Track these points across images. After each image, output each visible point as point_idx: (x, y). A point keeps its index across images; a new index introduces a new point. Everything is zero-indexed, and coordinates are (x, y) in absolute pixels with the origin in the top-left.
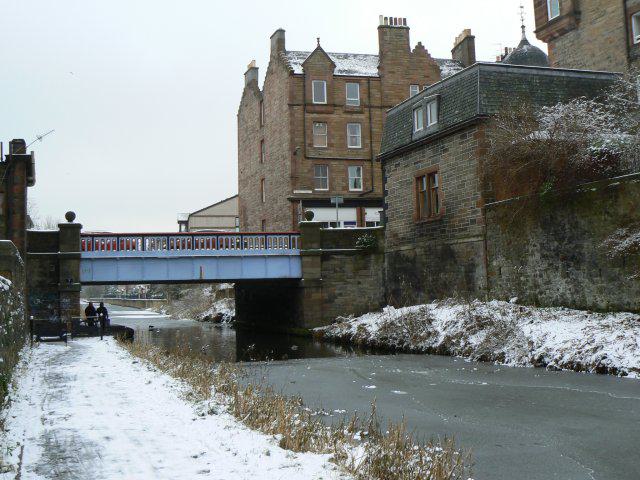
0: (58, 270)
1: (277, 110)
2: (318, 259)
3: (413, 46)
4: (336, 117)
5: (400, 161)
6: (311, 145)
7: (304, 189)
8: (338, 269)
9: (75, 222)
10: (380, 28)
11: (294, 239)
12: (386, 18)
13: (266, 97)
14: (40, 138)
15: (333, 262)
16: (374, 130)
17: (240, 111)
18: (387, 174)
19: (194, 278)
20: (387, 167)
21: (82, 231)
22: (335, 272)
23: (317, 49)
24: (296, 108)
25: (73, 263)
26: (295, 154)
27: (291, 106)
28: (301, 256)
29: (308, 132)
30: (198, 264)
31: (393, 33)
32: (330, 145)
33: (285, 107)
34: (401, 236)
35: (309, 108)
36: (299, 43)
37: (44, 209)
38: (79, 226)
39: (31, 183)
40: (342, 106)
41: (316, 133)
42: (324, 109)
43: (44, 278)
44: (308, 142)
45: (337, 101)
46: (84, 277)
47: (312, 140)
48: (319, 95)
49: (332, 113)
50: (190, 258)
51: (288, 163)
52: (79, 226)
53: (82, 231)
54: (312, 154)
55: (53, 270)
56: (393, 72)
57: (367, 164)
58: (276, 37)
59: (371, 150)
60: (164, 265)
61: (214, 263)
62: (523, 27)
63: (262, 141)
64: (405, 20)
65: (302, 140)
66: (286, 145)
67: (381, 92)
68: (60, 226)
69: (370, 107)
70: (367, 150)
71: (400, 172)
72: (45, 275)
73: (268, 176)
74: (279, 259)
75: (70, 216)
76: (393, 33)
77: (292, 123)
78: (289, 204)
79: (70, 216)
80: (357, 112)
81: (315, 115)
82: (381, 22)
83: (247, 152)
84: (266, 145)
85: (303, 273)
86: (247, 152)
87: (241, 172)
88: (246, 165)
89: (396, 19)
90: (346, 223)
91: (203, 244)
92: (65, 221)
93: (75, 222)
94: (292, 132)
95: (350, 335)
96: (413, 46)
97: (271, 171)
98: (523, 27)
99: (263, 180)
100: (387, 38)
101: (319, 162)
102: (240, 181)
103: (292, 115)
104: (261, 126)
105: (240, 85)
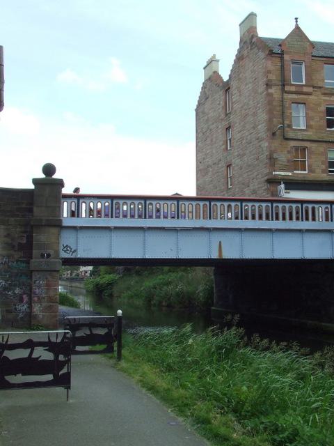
0: (30, 238)
6: (290, 126)
13: (234, 84)
29: (287, 113)
30: (216, 238)
32: (308, 126)
33: (262, 88)
36: (273, 28)
38: (60, 183)
40: (320, 88)
44: (287, 122)
47: (291, 122)
49: (309, 94)
52: (60, 183)
61: (236, 237)
66: (262, 127)
73: (236, 162)
74: (263, 234)
75: (49, 170)
77: (270, 103)
78: (266, 186)
79: (49, 170)
81: (294, 96)
83: (209, 141)
86: (209, 141)
87: (199, 162)
88: (206, 154)
91: (291, 214)
94: (270, 112)
97: (241, 156)
99: (229, 166)
100: (199, 144)
104: (227, 115)
105: (199, 79)
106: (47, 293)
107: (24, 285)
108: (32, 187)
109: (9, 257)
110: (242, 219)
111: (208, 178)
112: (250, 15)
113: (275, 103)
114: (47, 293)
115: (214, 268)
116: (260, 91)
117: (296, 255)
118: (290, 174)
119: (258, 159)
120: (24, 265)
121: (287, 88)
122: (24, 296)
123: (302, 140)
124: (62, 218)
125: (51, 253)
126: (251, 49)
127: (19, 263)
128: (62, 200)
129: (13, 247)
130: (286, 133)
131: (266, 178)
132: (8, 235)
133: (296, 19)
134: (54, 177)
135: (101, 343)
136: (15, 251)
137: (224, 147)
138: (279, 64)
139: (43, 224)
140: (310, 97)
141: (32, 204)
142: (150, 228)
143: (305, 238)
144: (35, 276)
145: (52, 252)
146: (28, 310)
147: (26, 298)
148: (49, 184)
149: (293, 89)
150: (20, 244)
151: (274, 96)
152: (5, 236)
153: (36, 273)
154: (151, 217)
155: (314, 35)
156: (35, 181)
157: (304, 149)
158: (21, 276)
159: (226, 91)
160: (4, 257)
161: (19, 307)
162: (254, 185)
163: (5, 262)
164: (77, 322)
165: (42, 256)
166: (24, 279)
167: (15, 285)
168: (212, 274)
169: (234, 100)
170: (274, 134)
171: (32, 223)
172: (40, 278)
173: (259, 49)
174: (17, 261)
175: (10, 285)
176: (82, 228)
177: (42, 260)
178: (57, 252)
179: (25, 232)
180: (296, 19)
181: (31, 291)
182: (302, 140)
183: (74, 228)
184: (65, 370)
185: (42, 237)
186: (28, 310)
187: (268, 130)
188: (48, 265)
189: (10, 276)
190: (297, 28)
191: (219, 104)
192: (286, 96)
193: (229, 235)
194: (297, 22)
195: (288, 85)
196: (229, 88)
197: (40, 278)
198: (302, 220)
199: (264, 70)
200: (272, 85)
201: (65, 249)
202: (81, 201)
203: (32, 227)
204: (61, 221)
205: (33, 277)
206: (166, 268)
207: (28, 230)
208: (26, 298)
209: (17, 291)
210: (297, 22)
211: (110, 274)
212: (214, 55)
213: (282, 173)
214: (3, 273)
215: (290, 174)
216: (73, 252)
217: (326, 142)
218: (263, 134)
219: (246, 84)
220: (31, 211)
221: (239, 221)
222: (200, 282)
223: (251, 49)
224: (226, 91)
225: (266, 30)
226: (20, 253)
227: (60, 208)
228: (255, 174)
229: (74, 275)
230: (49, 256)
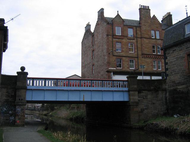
1: (101, 39)
3: (152, 16)
4: (124, 41)
5: (175, 48)
7: (113, 67)
8: (144, 97)
10: (140, 9)
11: (93, 82)
12: (142, 6)
13: (96, 34)
16: (138, 46)
17: (82, 41)
18: (167, 55)
20: (167, 52)
21: (28, 76)
22: (144, 98)
23: (117, 15)
24: (109, 36)
25: (23, 91)
26: (109, 54)
27: (107, 35)
28: (129, 91)
29: (114, 46)
30: (82, 94)
31: (144, 11)
32: (122, 51)
33: (105, 36)
34: (177, 82)
35: (114, 37)
36: (109, 14)
38: (27, 74)
39: (4, 51)
41: (117, 46)
42: (120, 37)
43: (8, 98)
44: (114, 49)
45: (125, 35)
46: (28, 98)
48: (118, 32)
50: (79, 90)
51: (106, 57)
52: (27, 74)
53: (28, 76)
54: (116, 54)
56: (145, 25)
57: (136, 59)
58: (101, 12)
59: (138, 54)
60: (66, 93)
61: (89, 93)
62: (187, 13)
63: (93, 51)
64: (148, 7)
65: (112, 48)
66: (105, 51)
67: (141, 32)
69: (137, 37)
70: (136, 53)
71: (176, 53)
73: (96, 64)
75: (23, 68)
76: (144, 11)
77: (108, 42)
78: (107, 73)
79: (23, 68)
80: (132, 39)
81: (117, 40)
82: (140, 7)
84: (95, 52)
85: (130, 99)
87: (82, 63)
89: (145, 6)
91: (120, 86)
94: (108, 45)
95: (177, 129)
96: (152, 16)
97: (97, 61)
98: (187, 13)
99: (93, 65)
100: (143, 13)
101: (118, 57)
102: (82, 67)
103: (108, 39)
104: (93, 45)
105: (83, 32)
108: (17, 75)
110: (124, 87)
111: (86, 70)
112: (101, 9)
116: (105, 37)
117: (100, 100)
118: (115, 69)
119: (103, 63)
128: (27, 80)
130: (114, 53)
131: (106, 70)
132: (7, 92)
133: (118, 11)
134: (25, 71)
135: (40, 103)
137: (91, 58)
140: (123, 40)
142: (59, 90)
143: (114, 94)
144: (17, 107)
148: (23, 74)
154: (82, 86)
155: (123, 17)
156: (18, 73)
162: (102, 73)
167: (10, 110)
168: (85, 107)
169: (95, 40)
180: (118, 11)
183: (31, 90)
185: (18, 93)
190: (118, 15)
191: (90, 41)
192: (114, 40)
193: (87, 93)
194: (118, 12)
198: (124, 87)
202: (34, 80)
210: (118, 12)
212: (89, 22)
213: (112, 69)
215: (115, 69)
217: (129, 57)
218: (105, 54)
219: (100, 34)
220: (16, 83)
221: (79, 87)
224: (93, 36)
225: (106, 15)
230: (22, 99)
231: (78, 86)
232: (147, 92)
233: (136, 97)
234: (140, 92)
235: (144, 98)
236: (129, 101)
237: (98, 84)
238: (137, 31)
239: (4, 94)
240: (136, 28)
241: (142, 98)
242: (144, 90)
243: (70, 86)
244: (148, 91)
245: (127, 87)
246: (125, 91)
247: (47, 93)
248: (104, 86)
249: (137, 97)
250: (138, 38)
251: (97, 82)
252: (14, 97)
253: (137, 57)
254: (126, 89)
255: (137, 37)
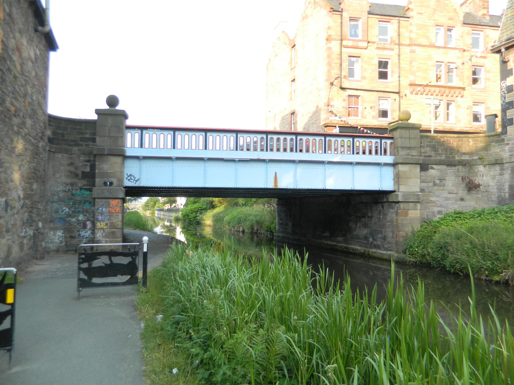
0: (93, 167)
2: (418, 168)
8: (438, 182)
9: (119, 108)
14: (464, 51)
15: (432, 172)
19: (268, 187)
21: (129, 122)
22: (435, 184)
28: (394, 165)
30: (273, 168)
37: (71, 93)
43: (75, 180)
52: (124, 115)
53: (129, 122)
55: (88, 169)
68: (98, 112)
72: (77, 175)
75: (112, 101)
77: (329, 56)
79: (112, 101)
90: (436, 132)
92: (105, 106)
93: (119, 108)
94: (329, 64)
106: (109, 220)
107: (87, 212)
108: (95, 117)
109: (72, 184)
110: (381, 154)
113: (333, 57)
114: (109, 220)
115: (277, 200)
120: (88, 193)
121: (345, 43)
122: (88, 223)
123: (357, 90)
124: (125, 149)
125: (113, 181)
126: (315, 8)
127: (83, 191)
129: (77, 175)
134: (118, 108)
136: (79, 179)
138: (339, 21)
139: (106, 153)
141: (95, 134)
145: (114, 181)
146: (91, 236)
147: (89, 224)
148: (112, 116)
149: (350, 43)
150: (83, 173)
151: (333, 50)
152: (69, 165)
153: (99, 200)
156: (98, 112)
157: (358, 97)
158: (84, 203)
159: (293, 47)
160: (67, 184)
161: (83, 233)
163: (69, 190)
164: (95, 251)
165: (105, 184)
166: (87, 206)
167: (79, 212)
170: (332, 84)
171: (94, 153)
172: (103, 205)
173: (321, 8)
174: (81, 189)
175: (74, 212)
176: (145, 158)
177: (104, 187)
178: (121, 180)
179: (89, 161)
181: (94, 218)
182: (357, 90)
184: (6, 324)
185: (107, 166)
186: (91, 236)
187: (327, 80)
188: (110, 193)
189: (74, 204)
195: (346, 39)
196: (295, 45)
197: (103, 205)
198: (381, 154)
199: (323, 8)
200: (331, 40)
201: (129, 178)
203: (95, 156)
204: (124, 151)
205: (96, 204)
206: (241, 201)
207: (92, 159)
208: (89, 224)
209: (81, 217)
211: (94, 185)
214: (67, 201)
216: (136, 181)
220: (94, 140)
222: (261, 210)
223: (315, 8)
226: (84, 181)
227: (122, 137)
228: (314, 120)
229: (172, 206)
230: (111, 184)
231: (292, 150)
232: (444, 167)
233: (413, 183)
234: (424, 167)
235: (435, 184)
236: (394, 191)
237: (314, 144)
238: (401, 30)
239: (62, 168)
240: (399, 22)
241: (431, 184)
242: (440, 163)
243: (248, 150)
244: (448, 165)
245: (390, 155)
246: (386, 164)
247: (212, 166)
248: (330, 149)
249: (419, 180)
250: (404, 45)
251: (282, 137)
252: (90, 176)
253: (397, 91)
254: (389, 159)
255: (399, 45)
